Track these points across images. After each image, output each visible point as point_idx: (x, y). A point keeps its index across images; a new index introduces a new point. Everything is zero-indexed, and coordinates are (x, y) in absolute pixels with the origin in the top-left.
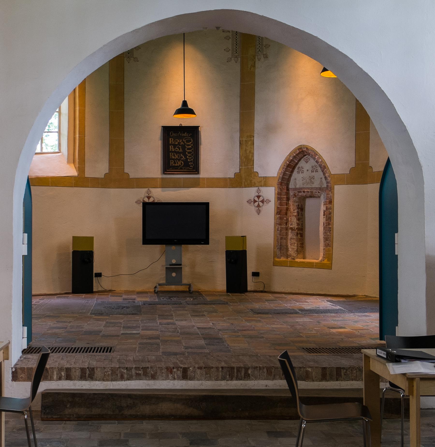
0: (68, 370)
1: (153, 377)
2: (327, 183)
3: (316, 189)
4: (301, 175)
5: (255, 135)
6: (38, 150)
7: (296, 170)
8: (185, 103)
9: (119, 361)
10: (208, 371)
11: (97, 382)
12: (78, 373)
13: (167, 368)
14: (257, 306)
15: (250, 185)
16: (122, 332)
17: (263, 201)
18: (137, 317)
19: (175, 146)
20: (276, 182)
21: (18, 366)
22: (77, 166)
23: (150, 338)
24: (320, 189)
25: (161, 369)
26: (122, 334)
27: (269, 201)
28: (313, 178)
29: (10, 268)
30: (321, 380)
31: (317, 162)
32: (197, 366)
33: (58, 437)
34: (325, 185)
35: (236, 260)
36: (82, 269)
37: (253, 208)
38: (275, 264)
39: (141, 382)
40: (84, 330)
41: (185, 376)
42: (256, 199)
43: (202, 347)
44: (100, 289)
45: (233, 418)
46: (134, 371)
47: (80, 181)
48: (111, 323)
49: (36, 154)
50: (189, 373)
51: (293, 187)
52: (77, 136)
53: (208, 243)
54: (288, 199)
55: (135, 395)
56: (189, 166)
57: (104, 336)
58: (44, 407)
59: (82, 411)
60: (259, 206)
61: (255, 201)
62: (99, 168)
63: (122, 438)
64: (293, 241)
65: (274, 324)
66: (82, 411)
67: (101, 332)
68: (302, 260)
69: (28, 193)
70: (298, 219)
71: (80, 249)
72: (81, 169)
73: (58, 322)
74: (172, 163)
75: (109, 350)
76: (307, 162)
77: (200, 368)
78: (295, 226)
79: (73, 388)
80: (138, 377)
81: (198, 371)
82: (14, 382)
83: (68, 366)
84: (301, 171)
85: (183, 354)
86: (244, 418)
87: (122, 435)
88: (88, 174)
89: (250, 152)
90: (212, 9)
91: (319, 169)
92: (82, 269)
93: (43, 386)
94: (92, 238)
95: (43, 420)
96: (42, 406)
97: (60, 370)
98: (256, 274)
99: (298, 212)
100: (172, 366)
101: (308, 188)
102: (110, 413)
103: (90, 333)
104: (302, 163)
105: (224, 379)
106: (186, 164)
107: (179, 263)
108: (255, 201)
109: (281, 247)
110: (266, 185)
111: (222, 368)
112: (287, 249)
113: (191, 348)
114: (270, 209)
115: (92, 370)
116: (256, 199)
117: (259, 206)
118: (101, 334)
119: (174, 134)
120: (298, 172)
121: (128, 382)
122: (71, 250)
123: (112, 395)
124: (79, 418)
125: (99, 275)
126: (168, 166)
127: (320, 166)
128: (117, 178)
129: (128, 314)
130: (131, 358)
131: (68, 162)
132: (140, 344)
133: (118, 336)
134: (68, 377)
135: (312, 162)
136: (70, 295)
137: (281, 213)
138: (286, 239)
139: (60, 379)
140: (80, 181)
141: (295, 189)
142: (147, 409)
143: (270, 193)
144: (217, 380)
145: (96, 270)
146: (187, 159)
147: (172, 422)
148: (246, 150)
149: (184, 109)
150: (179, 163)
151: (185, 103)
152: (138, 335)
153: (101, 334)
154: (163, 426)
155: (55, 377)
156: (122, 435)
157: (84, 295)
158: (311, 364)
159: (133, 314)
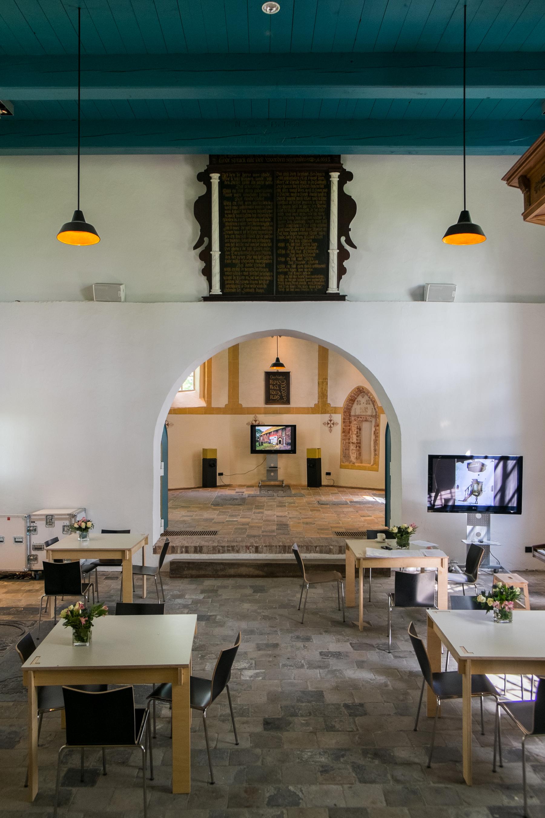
0: (187, 547)
1: (238, 552)
2: (376, 412)
3: (369, 416)
4: (359, 406)
5: (329, 378)
6: (180, 390)
7: (356, 402)
8: (278, 359)
9: (218, 541)
10: (270, 548)
11: (204, 555)
12: (193, 549)
13: (246, 546)
14: (324, 498)
15: (324, 412)
16: (227, 519)
17: (333, 424)
18: (241, 507)
19: (273, 385)
20: (342, 411)
21: (157, 545)
22: (206, 399)
23: (243, 525)
24: (372, 416)
25: (243, 547)
26: (227, 521)
27: (337, 424)
28: (367, 408)
29: (151, 486)
30: (339, 554)
31: (369, 397)
32: (264, 545)
33: (178, 588)
34: (374, 414)
35: (314, 466)
36: (209, 472)
37: (326, 428)
38: (341, 467)
39: (230, 554)
40: (203, 518)
41: (257, 550)
42: (329, 422)
43: (273, 531)
44: (222, 484)
45: (283, 577)
46: (226, 548)
47: (208, 410)
48: (222, 512)
49: (179, 391)
50: (259, 549)
51: (354, 414)
52: (206, 379)
53: (295, 453)
54: (350, 422)
55: (225, 563)
56: (283, 399)
57: (215, 523)
58: (171, 570)
59: (194, 572)
60: (331, 427)
61: (328, 424)
62: (221, 400)
63: (215, 588)
64: (354, 451)
65: (327, 513)
66: (194, 572)
67: (213, 519)
68: (360, 464)
69: (165, 434)
70: (357, 436)
71: (209, 457)
72: (209, 402)
73: (188, 511)
74: (271, 397)
75: (215, 533)
76: (363, 397)
77: (266, 546)
78: (355, 440)
79: (189, 558)
80: (229, 551)
81: (265, 548)
82: (154, 555)
83: (187, 545)
84: (359, 403)
85: (259, 536)
86: (287, 577)
87: (215, 587)
88: (213, 405)
89: (325, 389)
90: (274, 329)
91: (371, 402)
92: (209, 472)
93: (169, 558)
94: (216, 450)
95: (171, 577)
96: (170, 569)
97: (182, 547)
98: (328, 474)
99: (357, 432)
100: (249, 545)
101: (364, 415)
102: (210, 573)
103: (206, 520)
104: (360, 398)
105: (280, 553)
106: (281, 397)
107: (276, 466)
108: (328, 424)
109: (345, 455)
110: (335, 413)
111: (279, 546)
112: (349, 457)
113: (266, 532)
114: (338, 429)
115: (201, 548)
116: (329, 422)
117: (331, 427)
118: (213, 521)
119: (273, 377)
120: (357, 404)
121: (223, 555)
122: (202, 458)
123: (211, 563)
124: (192, 577)
125: (221, 474)
126: (269, 400)
127: (371, 400)
128: (234, 408)
129: (235, 505)
130: (226, 540)
131: (200, 397)
132: (236, 529)
133: (223, 523)
134: (187, 552)
135: (366, 398)
136: (201, 489)
137: (346, 432)
138: (349, 450)
139: (182, 553)
140: (208, 410)
141: (355, 416)
142: (232, 571)
143: (338, 418)
144: (276, 553)
145: (218, 471)
146: (282, 394)
147: (247, 579)
148: (322, 388)
149: (278, 363)
150: (277, 397)
151: (278, 359)
152: (236, 522)
153: (213, 521)
154: (240, 581)
155: (179, 552)
156: (215, 587)
157: (210, 489)
158: (334, 543)
159: (239, 505)
